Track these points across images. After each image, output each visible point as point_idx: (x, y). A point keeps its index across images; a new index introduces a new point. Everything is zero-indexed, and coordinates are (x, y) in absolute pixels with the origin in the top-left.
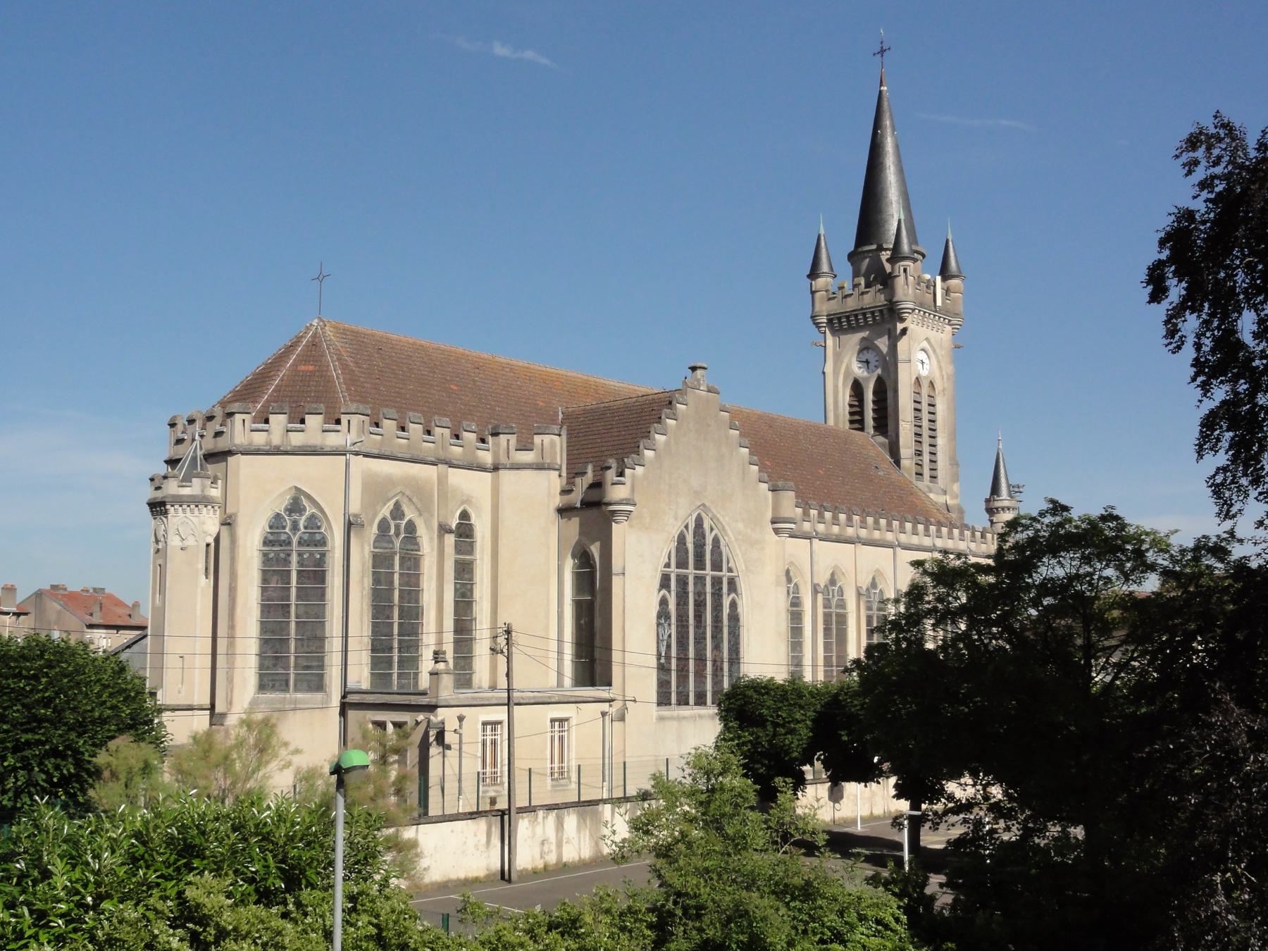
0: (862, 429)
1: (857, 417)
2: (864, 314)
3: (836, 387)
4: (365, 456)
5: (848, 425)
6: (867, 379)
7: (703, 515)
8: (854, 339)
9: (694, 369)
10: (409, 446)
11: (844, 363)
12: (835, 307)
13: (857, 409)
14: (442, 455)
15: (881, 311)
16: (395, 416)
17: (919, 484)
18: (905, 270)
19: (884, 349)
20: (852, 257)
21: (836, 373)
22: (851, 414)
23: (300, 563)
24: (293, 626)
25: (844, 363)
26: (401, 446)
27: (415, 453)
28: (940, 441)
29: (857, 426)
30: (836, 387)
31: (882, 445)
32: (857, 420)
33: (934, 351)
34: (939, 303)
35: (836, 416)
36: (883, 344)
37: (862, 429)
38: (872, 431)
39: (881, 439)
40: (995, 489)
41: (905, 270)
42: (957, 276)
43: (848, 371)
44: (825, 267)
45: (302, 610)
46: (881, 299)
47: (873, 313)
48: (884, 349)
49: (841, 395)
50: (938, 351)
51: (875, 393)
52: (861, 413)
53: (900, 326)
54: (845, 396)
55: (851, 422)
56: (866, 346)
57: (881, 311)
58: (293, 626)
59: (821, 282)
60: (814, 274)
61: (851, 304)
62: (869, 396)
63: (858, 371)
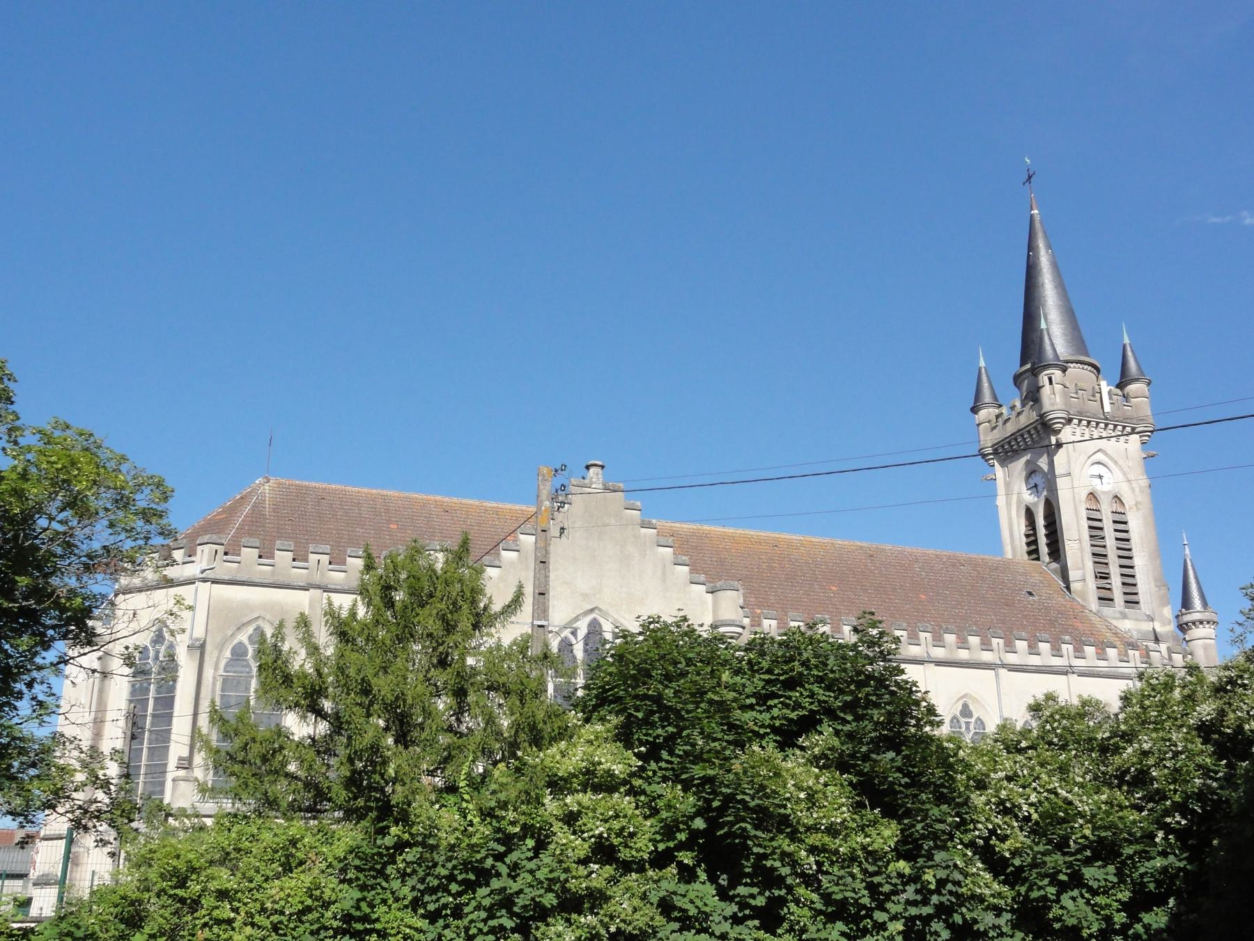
0: (1038, 559)
1: (1033, 547)
2: (1022, 435)
3: (1010, 518)
4: (213, 582)
5: (1026, 557)
6: (1036, 504)
7: (602, 621)
8: (1020, 465)
9: (588, 467)
10: (273, 573)
11: (1011, 492)
12: (997, 436)
13: (1032, 538)
14: (317, 579)
15: (1035, 428)
16: (257, 544)
17: (1107, 611)
18: (1050, 379)
19: (1045, 468)
20: (1017, 379)
21: (1008, 504)
22: (1028, 544)
23: (158, 691)
24: (145, 751)
25: (1011, 492)
26: (261, 572)
27: (281, 579)
28: (1140, 561)
29: (1034, 556)
30: (1010, 518)
31: (1054, 571)
32: (1034, 553)
33: (1116, 462)
34: (1107, 408)
35: (1013, 549)
36: (1043, 463)
37: (1038, 559)
38: (1047, 559)
39: (1055, 565)
40: (1186, 603)
41: (1050, 379)
42: (1137, 380)
43: (1019, 502)
44: (987, 397)
45: (154, 737)
46: (1034, 416)
47: (1029, 432)
48: (1045, 468)
49: (1015, 527)
50: (1121, 462)
51: (1046, 518)
52: (1035, 542)
53: (1053, 440)
54: (1021, 527)
55: (1029, 553)
56: (1032, 471)
57: (1035, 428)
58: (145, 751)
59: (983, 414)
60: (975, 410)
61: (1011, 428)
62: (1040, 522)
63: (1029, 498)
